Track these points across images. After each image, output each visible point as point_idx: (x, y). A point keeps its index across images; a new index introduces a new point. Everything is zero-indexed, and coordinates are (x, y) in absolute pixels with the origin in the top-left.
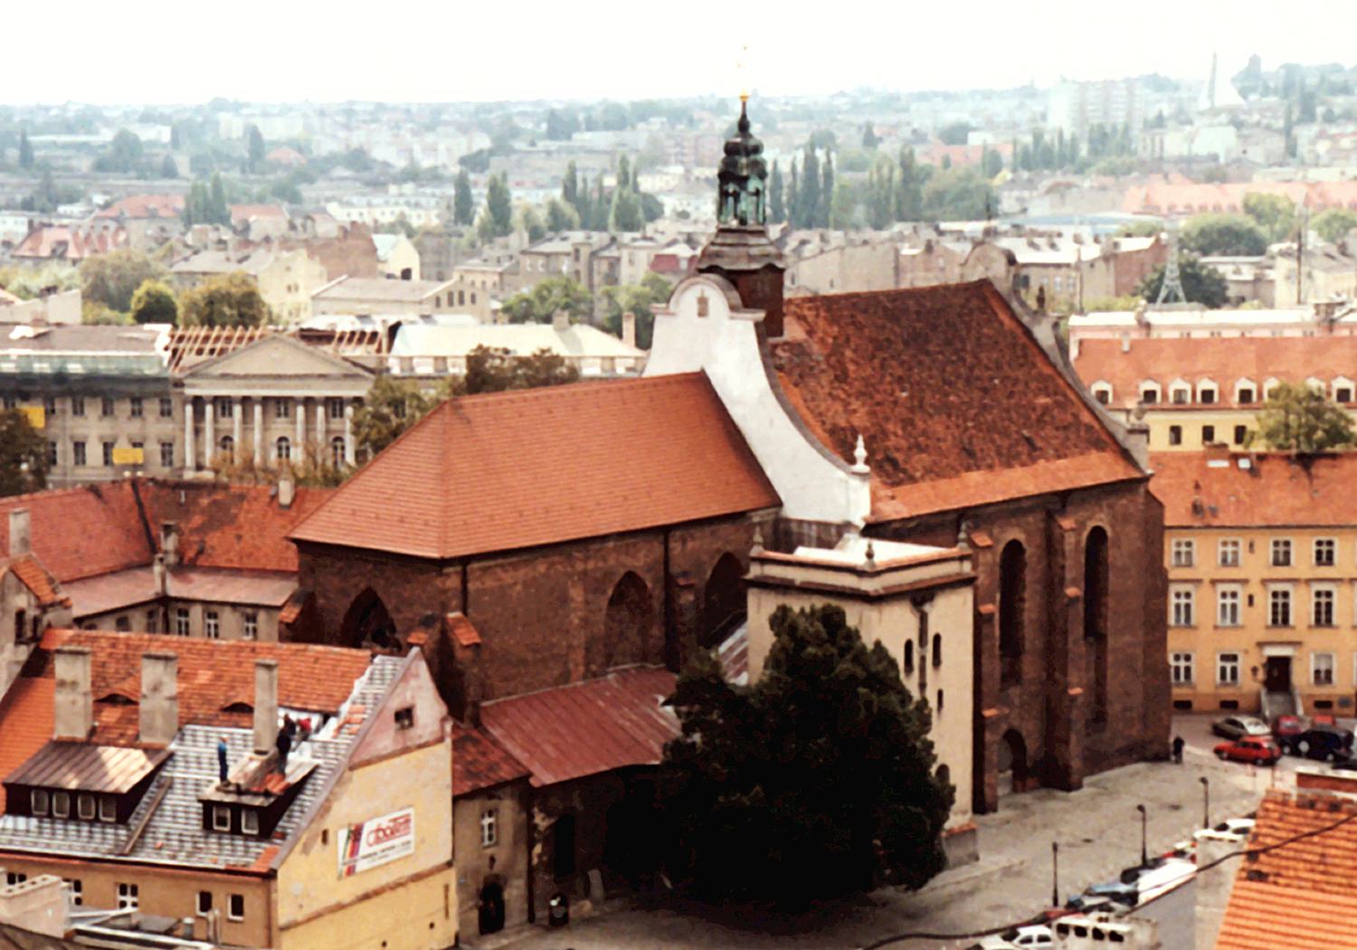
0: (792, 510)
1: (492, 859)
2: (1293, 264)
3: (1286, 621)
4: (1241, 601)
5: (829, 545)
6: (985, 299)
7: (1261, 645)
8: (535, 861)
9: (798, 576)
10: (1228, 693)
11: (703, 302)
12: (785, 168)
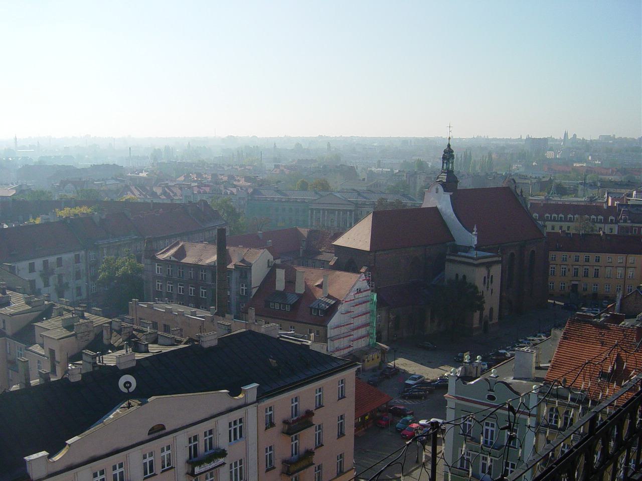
0: (458, 242)
1: (379, 325)
2: (582, 186)
4: (567, 269)
8: (390, 326)
11: (437, 189)
12: (459, 156)
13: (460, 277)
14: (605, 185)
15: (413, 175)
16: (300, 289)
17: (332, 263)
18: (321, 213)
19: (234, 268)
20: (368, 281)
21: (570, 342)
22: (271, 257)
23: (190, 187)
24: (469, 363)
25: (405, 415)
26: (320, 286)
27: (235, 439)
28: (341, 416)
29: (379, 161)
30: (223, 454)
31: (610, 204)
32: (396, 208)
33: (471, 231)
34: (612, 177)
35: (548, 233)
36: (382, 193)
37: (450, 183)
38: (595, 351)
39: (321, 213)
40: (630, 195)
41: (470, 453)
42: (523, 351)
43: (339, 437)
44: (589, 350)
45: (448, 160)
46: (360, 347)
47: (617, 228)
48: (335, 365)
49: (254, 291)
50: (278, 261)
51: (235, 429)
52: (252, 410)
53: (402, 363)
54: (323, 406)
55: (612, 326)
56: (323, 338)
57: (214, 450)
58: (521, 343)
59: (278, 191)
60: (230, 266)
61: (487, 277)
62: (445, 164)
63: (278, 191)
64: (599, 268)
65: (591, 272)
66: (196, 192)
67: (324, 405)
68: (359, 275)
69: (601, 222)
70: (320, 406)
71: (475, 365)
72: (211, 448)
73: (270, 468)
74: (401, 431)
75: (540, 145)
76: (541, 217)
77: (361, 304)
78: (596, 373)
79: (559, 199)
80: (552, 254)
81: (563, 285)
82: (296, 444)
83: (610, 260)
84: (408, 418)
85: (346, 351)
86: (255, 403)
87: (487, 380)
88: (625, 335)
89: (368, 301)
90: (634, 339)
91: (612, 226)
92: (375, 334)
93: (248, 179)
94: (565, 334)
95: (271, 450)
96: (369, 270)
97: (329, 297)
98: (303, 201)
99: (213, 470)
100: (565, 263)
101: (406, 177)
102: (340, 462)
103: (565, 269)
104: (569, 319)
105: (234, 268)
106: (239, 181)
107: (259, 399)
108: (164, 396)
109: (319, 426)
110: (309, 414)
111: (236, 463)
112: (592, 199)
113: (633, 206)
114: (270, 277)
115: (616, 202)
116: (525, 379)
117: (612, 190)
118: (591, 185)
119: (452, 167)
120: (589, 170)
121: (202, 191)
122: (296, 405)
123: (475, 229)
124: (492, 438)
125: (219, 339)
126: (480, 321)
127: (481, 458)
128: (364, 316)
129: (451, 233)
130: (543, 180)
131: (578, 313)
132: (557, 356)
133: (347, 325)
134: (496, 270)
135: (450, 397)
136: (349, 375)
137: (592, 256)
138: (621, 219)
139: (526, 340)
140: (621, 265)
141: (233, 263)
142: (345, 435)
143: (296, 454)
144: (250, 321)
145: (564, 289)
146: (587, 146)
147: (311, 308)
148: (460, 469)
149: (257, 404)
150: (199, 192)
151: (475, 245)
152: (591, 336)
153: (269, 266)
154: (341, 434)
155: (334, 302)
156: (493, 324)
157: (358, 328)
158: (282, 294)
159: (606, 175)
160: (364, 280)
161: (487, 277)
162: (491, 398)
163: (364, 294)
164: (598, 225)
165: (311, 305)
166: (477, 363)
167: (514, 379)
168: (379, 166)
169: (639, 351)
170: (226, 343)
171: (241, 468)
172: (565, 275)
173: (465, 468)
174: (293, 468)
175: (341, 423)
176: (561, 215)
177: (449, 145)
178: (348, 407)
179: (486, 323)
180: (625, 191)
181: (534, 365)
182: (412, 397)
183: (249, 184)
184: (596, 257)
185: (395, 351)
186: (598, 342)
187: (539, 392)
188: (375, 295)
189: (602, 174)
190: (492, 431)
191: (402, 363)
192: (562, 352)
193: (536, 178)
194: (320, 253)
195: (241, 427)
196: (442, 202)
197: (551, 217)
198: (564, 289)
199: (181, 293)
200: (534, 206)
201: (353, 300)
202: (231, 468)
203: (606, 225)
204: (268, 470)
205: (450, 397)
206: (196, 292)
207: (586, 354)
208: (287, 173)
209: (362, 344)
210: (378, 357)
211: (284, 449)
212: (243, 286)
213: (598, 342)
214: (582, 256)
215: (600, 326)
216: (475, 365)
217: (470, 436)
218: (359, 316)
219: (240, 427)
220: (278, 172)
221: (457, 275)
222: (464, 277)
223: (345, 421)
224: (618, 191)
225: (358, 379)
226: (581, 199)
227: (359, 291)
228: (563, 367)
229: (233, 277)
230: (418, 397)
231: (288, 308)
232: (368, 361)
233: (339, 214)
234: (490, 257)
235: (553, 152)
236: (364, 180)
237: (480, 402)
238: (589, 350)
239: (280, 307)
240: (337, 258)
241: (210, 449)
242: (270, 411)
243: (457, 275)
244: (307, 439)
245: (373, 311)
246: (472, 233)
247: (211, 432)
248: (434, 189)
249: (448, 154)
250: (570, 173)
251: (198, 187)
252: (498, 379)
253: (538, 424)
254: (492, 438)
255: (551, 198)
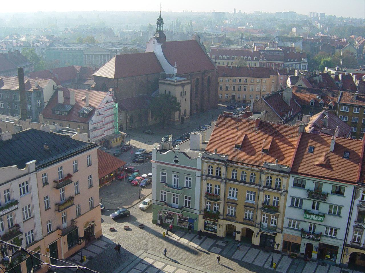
0: (166, 73)
3: (235, 90)
4: (229, 87)
5: (171, 78)
6: (265, 132)
7: (231, 93)
8: (127, 122)
9: (166, 82)
10: (227, 100)
11: (154, 42)
13: (167, 92)
14: (253, 39)
15: (146, 33)
16: (72, 102)
17: (93, 86)
18: (91, 57)
19: (33, 91)
20: (112, 96)
21: (220, 128)
22: (55, 84)
23: (11, 43)
24: (164, 142)
25: (134, 172)
26: (84, 100)
27: (24, 193)
28: (90, 176)
29: (127, 26)
30: (16, 202)
31: (255, 50)
32: (133, 53)
33: (173, 66)
34: (259, 35)
35: (218, 66)
36: (127, 44)
37: (161, 38)
38: (233, 133)
39: (91, 57)
40: (266, 45)
41: (166, 193)
42: (195, 134)
43: (89, 188)
44: (230, 133)
45: (160, 24)
46: (109, 134)
47: (258, 63)
48: (84, 147)
49: (46, 104)
50: (60, 86)
51: (24, 188)
52: (33, 176)
53: (132, 142)
54: (78, 171)
55: (243, 119)
56: (87, 131)
57: (11, 201)
58: (202, 128)
59: (64, 44)
60: (31, 90)
61: (182, 92)
62: (158, 27)
63: (64, 44)
64: (246, 86)
65: (242, 88)
66: (15, 46)
67: (78, 170)
68: (107, 93)
69: (250, 60)
70: (77, 171)
71: (168, 142)
72: (9, 199)
73: (48, 208)
74: (131, 182)
75: (220, 16)
76: (216, 58)
77: (108, 109)
78: (233, 145)
79: (228, 47)
80: (220, 78)
81: (221, 95)
82: (63, 193)
83: (253, 82)
84: (135, 174)
85: (101, 137)
86: (34, 172)
87: (173, 151)
88: (250, 124)
89: (113, 108)
90: (255, 126)
91: (256, 62)
92: (118, 127)
93: (48, 37)
94: (217, 124)
95: (47, 197)
96: (114, 90)
97: (90, 106)
98: (80, 50)
99: (12, 212)
100: (229, 83)
101: (142, 35)
102: (92, 202)
103: (228, 86)
104: (220, 115)
105: (33, 91)
106: (42, 38)
107: (37, 169)
108: (4, 167)
109: (77, 182)
110: (70, 176)
111: (26, 207)
112: (245, 47)
113: (267, 51)
114: (55, 96)
115: (258, 49)
116: (196, 150)
117: (257, 42)
118: (246, 39)
119: (163, 29)
120: (247, 31)
121: (18, 45)
122: (61, 172)
123: (176, 64)
124: (177, 184)
125: (12, 135)
126: (179, 117)
127: (172, 195)
128: (111, 116)
129: (162, 67)
130: (219, 36)
131: (224, 112)
132: (213, 136)
133: (100, 122)
134: (188, 88)
135: (154, 161)
136: (94, 152)
137: (243, 79)
138: (261, 58)
139: (204, 126)
140: (258, 84)
141: (32, 88)
142: (93, 186)
143: (63, 199)
144: (41, 122)
145: (221, 97)
146: (247, 17)
147: (79, 113)
148: (161, 201)
149: (36, 172)
150: (17, 46)
151: (176, 74)
152: (231, 125)
153: (54, 89)
154: (91, 186)
155: (92, 109)
156: (186, 118)
157: (108, 123)
158: (62, 106)
159: (256, 33)
160: (109, 96)
161: (182, 92)
162: (176, 161)
163: (110, 104)
164: (248, 62)
165: (79, 111)
166: (169, 141)
167: (190, 150)
168: (127, 29)
169: (257, 133)
170: (18, 137)
171: (29, 210)
172: (228, 90)
173: (164, 201)
174: (62, 208)
175: (91, 180)
176: (228, 56)
177: (160, 16)
178: (94, 171)
179: (182, 118)
180: (264, 43)
181: (201, 142)
182: (138, 162)
183: (49, 40)
184: (239, 79)
185: (129, 136)
186: (235, 128)
187: (202, 157)
188: (117, 104)
189: (253, 33)
190: (178, 180)
191: (132, 142)
192: (215, 134)
193: (215, 35)
194: (86, 80)
195: (27, 187)
196: (157, 49)
197: (222, 58)
198: (227, 97)
199: (3, 107)
200: (213, 51)
201: (104, 107)
202: (23, 210)
203: (253, 61)
204: (46, 210)
205: (154, 161)
206: (11, 106)
207: (228, 135)
208: (72, 33)
209: (110, 132)
210: (120, 140)
211: (55, 197)
212: (39, 102)
213: (235, 128)
214: (237, 79)
215: (237, 120)
216: (168, 142)
217: (166, 183)
218: (108, 116)
219: (23, 188)
220: (67, 33)
221: (165, 91)
222: (170, 92)
223: (93, 178)
224: (261, 42)
225: (99, 155)
226: (239, 47)
227: (107, 102)
228: (215, 142)
229: (33, 96)
230: (143, 162)
231: (66, 114)
232: (114, 142)
233: (101, 57)
234: (185, 80)
235: (227, 20)
236: (117, 36)
237: (170, 164)
238: (230, 133)
239: (61, 113)
240: (96, 83)
241: (8, 200)
242: (45, 176)
243: (165, 91)
244: (69, 190)
245: (116, 113)
246: (174, 67)
247: (8, 190)
248: (152, 42)
249: (160, 22)
250: (236, 32)
251: (16, 42)
252: (180, 151)
253: (202, 175)
254: (177, 184)
255: (223, 46)
